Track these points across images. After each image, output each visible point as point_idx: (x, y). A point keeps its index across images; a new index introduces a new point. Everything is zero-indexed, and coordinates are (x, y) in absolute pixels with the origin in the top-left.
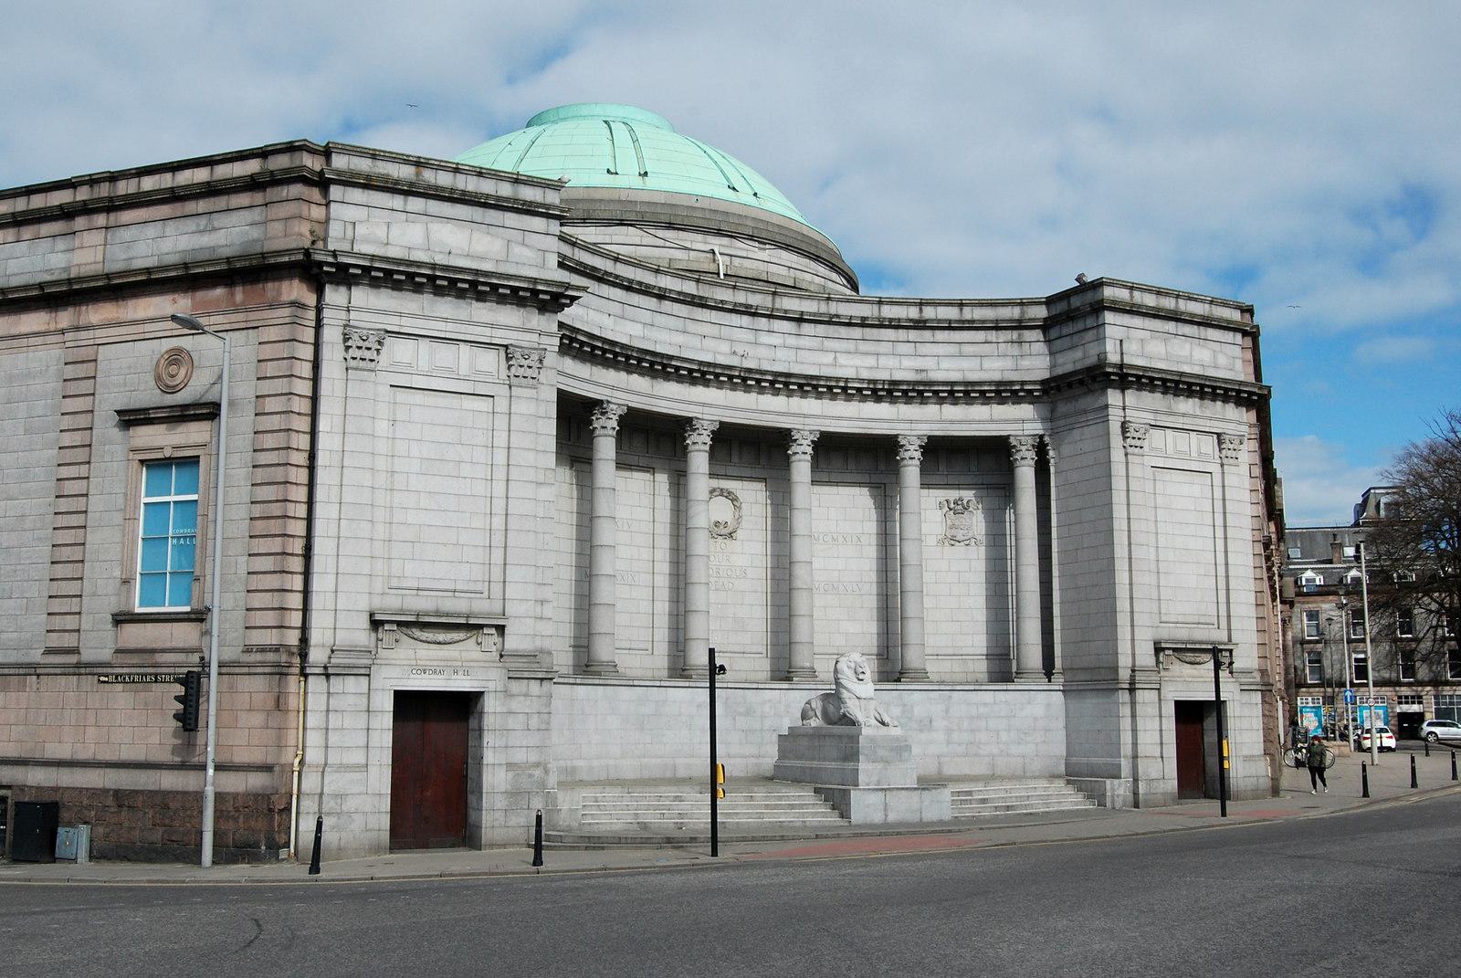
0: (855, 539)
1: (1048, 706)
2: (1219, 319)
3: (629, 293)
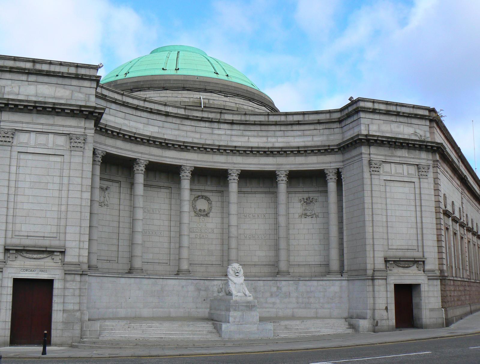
0: (263, 216)
1: (341, 287)
3: (136, 111)
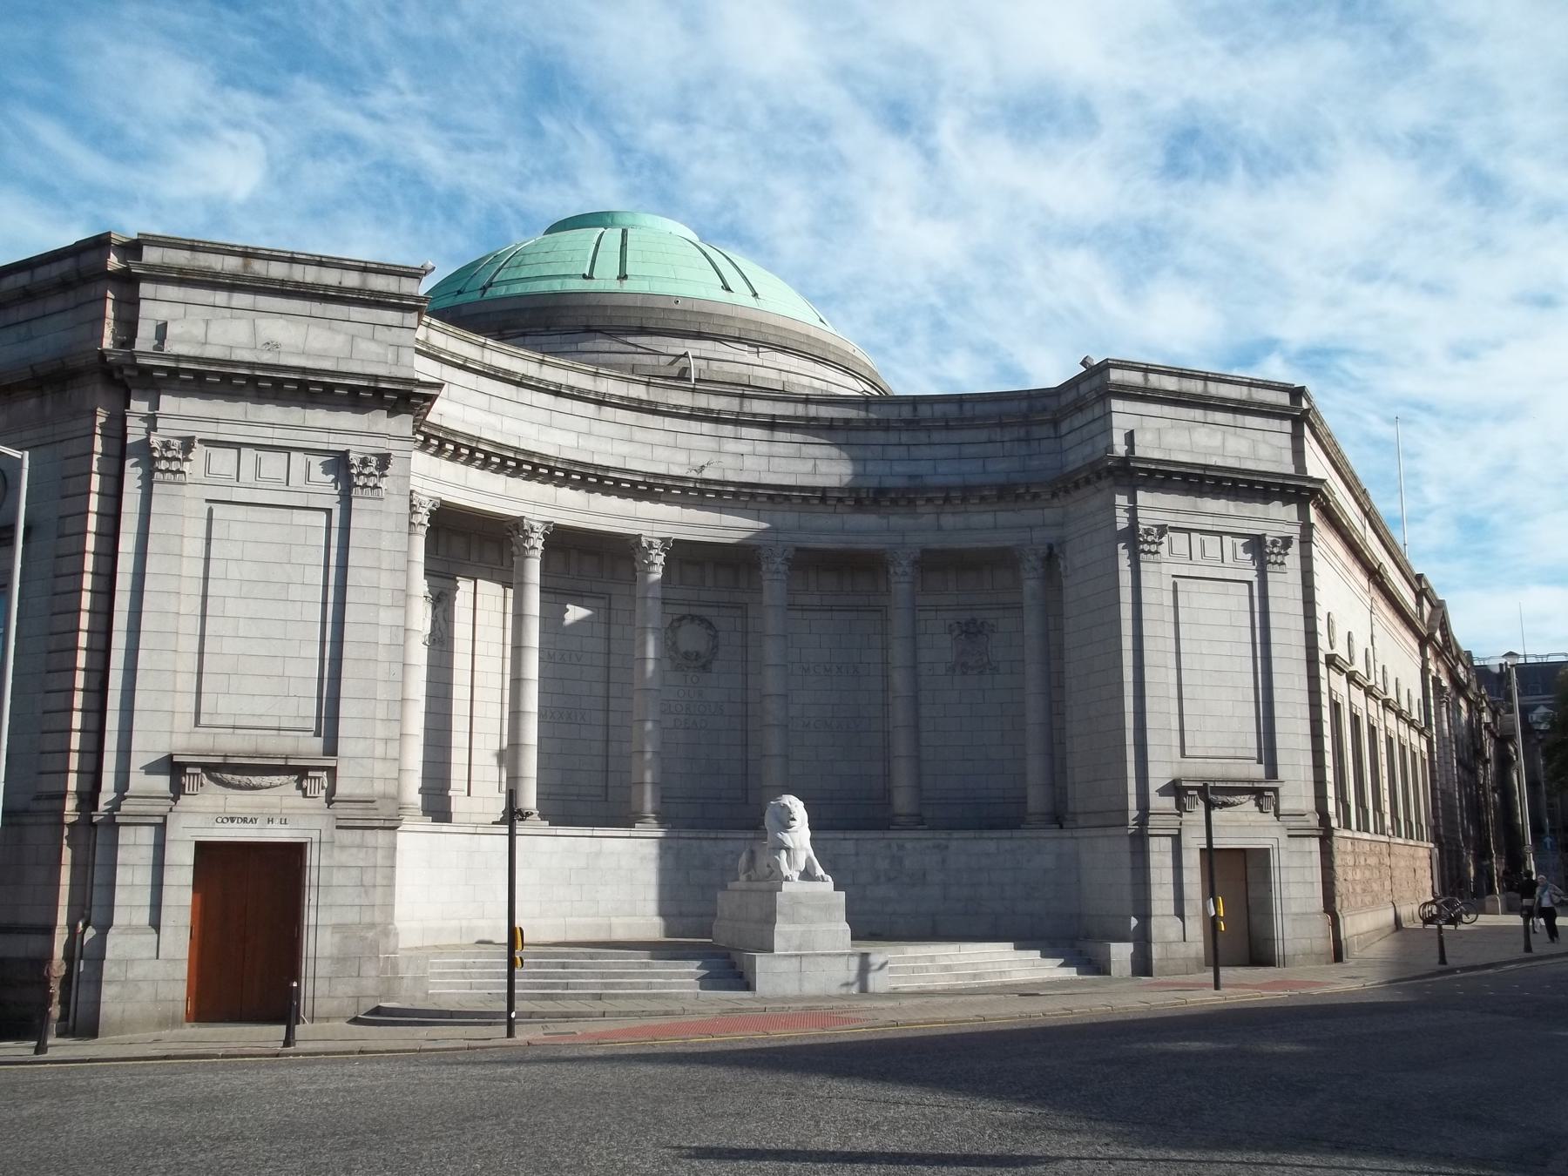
2: (1262, 404)
3: (559, 398)
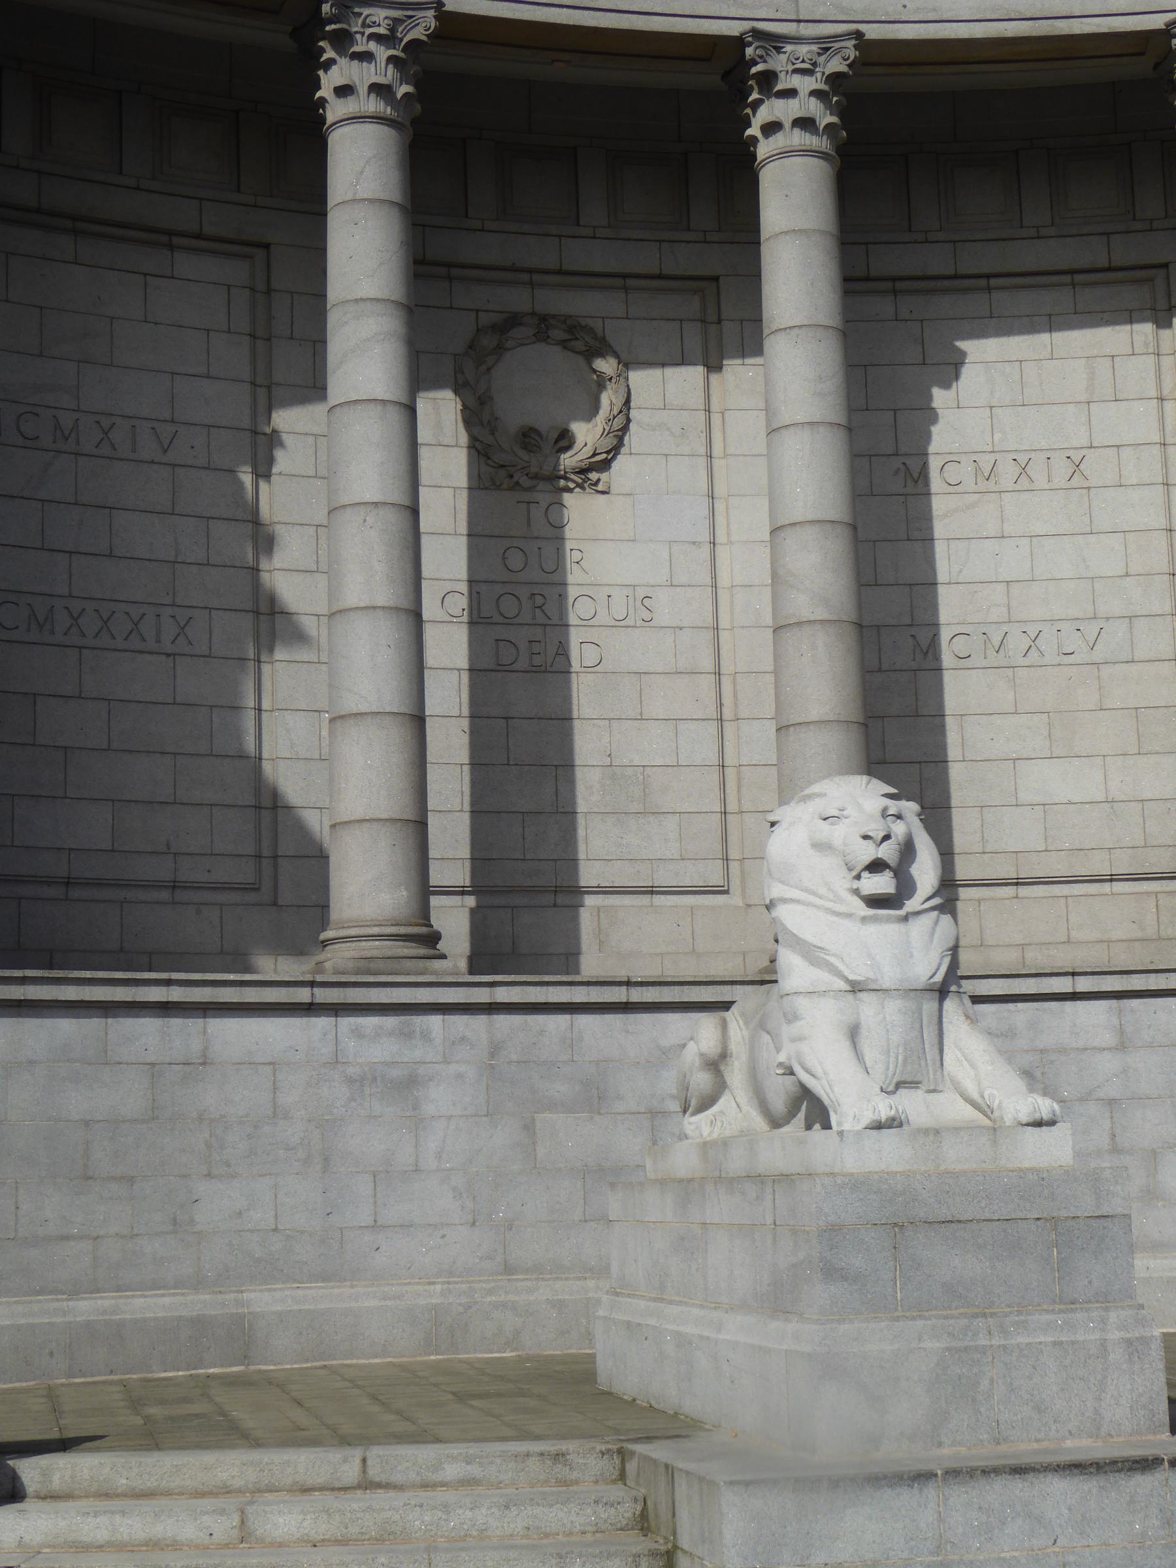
0: (1062, 469)
